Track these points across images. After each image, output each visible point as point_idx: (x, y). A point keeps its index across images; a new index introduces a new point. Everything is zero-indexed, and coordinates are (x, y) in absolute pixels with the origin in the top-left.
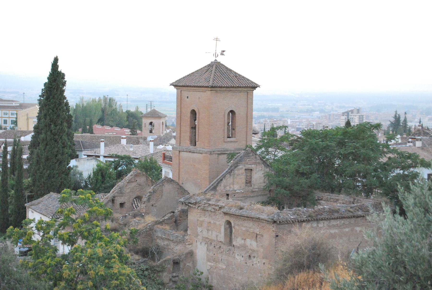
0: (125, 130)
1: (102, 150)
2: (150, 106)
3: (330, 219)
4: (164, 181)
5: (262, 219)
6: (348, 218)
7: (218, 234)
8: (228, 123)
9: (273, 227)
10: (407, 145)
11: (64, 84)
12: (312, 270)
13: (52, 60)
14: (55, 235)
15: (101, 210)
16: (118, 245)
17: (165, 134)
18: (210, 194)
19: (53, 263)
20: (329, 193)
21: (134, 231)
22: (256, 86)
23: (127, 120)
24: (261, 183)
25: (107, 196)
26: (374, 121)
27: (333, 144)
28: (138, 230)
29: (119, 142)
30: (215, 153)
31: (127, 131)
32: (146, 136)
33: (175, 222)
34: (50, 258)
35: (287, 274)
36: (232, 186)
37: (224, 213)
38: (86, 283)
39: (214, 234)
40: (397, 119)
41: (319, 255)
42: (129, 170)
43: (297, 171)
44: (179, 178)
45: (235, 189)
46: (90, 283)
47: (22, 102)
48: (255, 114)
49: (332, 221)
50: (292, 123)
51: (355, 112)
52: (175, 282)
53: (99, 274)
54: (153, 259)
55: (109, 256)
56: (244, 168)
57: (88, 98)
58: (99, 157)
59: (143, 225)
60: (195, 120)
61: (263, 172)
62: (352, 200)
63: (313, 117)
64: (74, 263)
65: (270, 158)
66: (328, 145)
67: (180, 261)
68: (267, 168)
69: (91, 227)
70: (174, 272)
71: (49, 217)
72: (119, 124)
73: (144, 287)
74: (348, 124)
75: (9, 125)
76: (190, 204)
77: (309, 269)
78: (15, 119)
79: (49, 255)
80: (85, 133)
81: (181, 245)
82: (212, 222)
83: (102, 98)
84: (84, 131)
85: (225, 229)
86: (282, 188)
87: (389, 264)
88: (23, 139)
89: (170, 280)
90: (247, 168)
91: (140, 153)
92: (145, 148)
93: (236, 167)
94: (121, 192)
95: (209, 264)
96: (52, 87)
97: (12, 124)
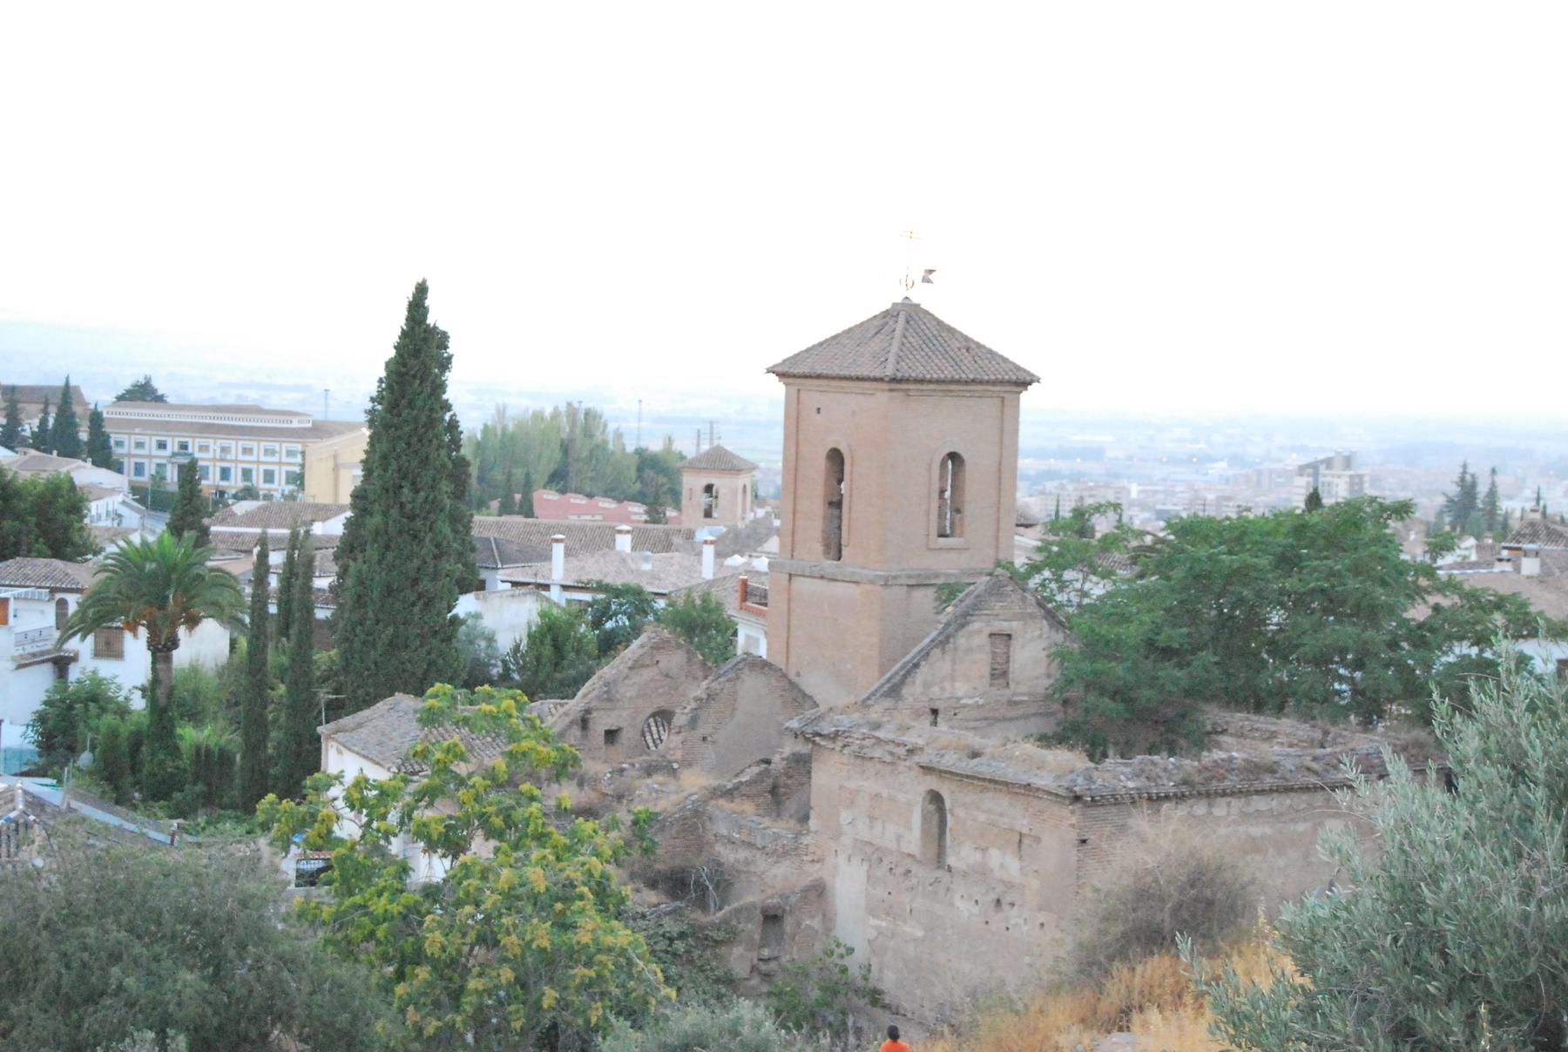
0: (630, 509)
1: (558, 568)
2: (708, 436)
4: (741, 666)
5: (1038, 789)
6: (1305, 789)
8: (942, 492)
13: (409, 292)
14: (402, 823)
15: (545, 750)
19: (395, 909)
21: (643, 816)
22: (1028, 379)
25: (567, 707)
26: (1391, 493)
27: (1264, 561)
28: (657, 814)
29: (611, 544)
32: (692, 526)
33: (774, 790)
34: (386, 894)
35: (1111, 959)
36: (947, 685)
37: (922, 767)
38: (494, 973)
40: (1468, 488)
41: (1210, 903)
42: (636, 631)
43: (1150, 644)
45: (960, 694)
46: (507, 974)
48: (1025, 464)
51: (1338, 463)
52: (767, 977)
54: (702, 903)
55: (567, 893)
56: (987, 631)
58: (546, 587)
59: (674, 798)
60: (840, 481)
61: (1045, 644)
62: (1318, 735)
65: (1069, 601)
66: (1248, 567)
67: (784, 910)
68: (1057, 631)
69: (512, 802)
71: (389, 769)
73: (668, 990)
74: (1314, 500)
75: (280, 487)
76: (817, 739)
78: (297, 469)
83: (563, 408)
84: (506, 509)
85: (925, 818)
86: (1102, 694)
87: (1395, 940)
88: (318, 529)
89: (753, 969)
90: (995, 630)
91: (673, 580)
93: (963, 626)
94: (609, 697)
95: (873, 922)
97: (288, 483)
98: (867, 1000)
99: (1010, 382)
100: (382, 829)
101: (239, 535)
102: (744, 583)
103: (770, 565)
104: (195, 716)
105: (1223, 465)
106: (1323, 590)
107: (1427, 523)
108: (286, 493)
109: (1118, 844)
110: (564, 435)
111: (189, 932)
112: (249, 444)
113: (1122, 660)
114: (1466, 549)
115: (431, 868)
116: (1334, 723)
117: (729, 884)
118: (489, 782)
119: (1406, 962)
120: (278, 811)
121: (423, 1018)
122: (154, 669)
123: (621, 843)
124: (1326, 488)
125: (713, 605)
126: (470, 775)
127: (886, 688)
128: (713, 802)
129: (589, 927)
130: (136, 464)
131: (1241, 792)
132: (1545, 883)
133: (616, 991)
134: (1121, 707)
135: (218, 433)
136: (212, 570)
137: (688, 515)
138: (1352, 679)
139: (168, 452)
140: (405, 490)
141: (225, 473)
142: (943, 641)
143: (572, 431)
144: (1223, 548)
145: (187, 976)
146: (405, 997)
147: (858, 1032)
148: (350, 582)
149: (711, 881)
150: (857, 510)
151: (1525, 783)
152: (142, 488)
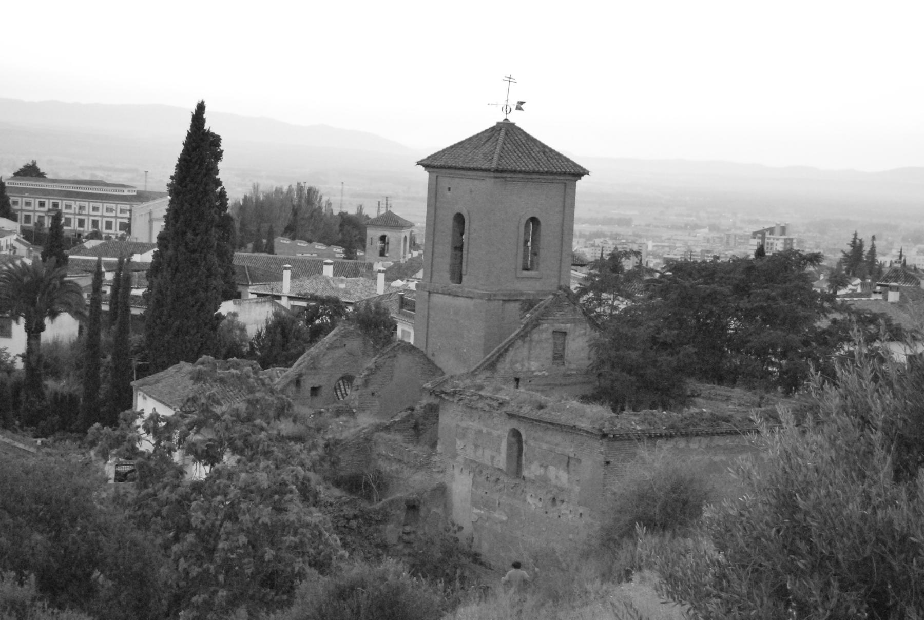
0: (335, 250)
1: (287, 285)
2: (384, 206)
3: (713, 434)
4: (396, 349)
5: (580, 429)
7: (494, 454)
8: (526, 242)
9: (602, 444)
10: (871, 299)
11: (218, 156)
12: (671, 532)
13: (193, 108)
14: (179, 443)
15: (271, 399)
16: (300, 468)
17: (409, 259)
18: (482, 376)
19: (174, 497)
20: (714, 384)
21: (332, 442)
22: (581, 172)
23: (341, 231)
24: (582, 359)
25: (287, 372)
26: (808, 248)
27: (726, 290)
28: (341, 441)
29: (320, 271)
30: (497, 298)
31: (338, 251)
32: (372, 262)
33: (415, 427)
34: (168, 488)
35: (621, 536)
36: (526, 365)
37: (509, 415)
38: (235, 539)
39: (488, 453)
40: (857, 246)
41: (685, 503)
42: (333, 326)
43: (654, 340)
44: (427, 346)
45: (533, 369)
46: (243, 539)
47: (141, 188)
48: (577, 227)
49: (717, 437)
50: (655, 249)
51: (778, 231)
52: (408, 543)
53: (260, 522)
54: (369, 498)
55: (281, 488)
56: (551, 330)
57: (268, 185)
58: (279, 297)
59: (352, 430)
60: (462, 234)
61: (586, 339)
62: (757, 399)
63: (696, 238)
64: (214, 499)
65: (604, 311)
66: (715, 292)
67: (420, 503)
68: (596, 330)
69: (249, 431)
70: (407, 524)
71: (175, 409)
72: (324, 238)
73: (344, 551)
74: (760, 252)
75: (116, 231)
76: (443, 395)
77: (664, 530)
78: (126, 221)
79: (167, 481)
80: (258, 251)
81: (423, 473)
82: (484, 431)
83: (294, 187)
84: (257, 249)
85: (510, 446)
86: (623, 370)
87: (778, 531)
88: (137, 258)
89: (400, 538)
91: (359, 294)
92: (367, 284)
93: (535, 326)
94: (314, 366)
95: (476, 511)
96: (191, 161)
97: (120, 229)
98: (471, 559)
99: (570, 174)
100: (167, 446)
101: (88, 261)
102: (402, 297)
103: (417, 286)
104: (56, 374)
105: (706, 230)
106: (762, 308)
107: (831, 269)
108: (119, 236)
109: (629, 465)
110: (295, 202)
111: (41, 510)
112: (82, 204)
113: (636, 349)
114: (855, 285)
115: (199, 472)
116: (767, 392)
117: (386, 486)
118: (234, 418)
119: (785, 547)
120: (101, 434)
121: (189, 566)
122: (29, 344)
123: (318, 458)
124: (769, 246)
125: (382, 311)
126: (223, 414)
127: (486, 365)
128: (376, 434)
129: (295, 510)
130: (25, 215)
131: (707, 434)
132: (879, 495)
133: (311, 551)
134: (633, 379)
135: (83, 198)
136: (70, 282)
137: (369, 254)
138: (780, 364)
139: (46, 209)
140: (189, 234)
141: (81, 223)
142: (523, 336)
143: (300, 201)
144: (701, 280)
145: (37, 537)
146: (179, 553)
147: (463, 579)
148: (154, 291)
149: (375, 482)
150: (472, 253)
151: (869, 428)
152: (29, 231)
